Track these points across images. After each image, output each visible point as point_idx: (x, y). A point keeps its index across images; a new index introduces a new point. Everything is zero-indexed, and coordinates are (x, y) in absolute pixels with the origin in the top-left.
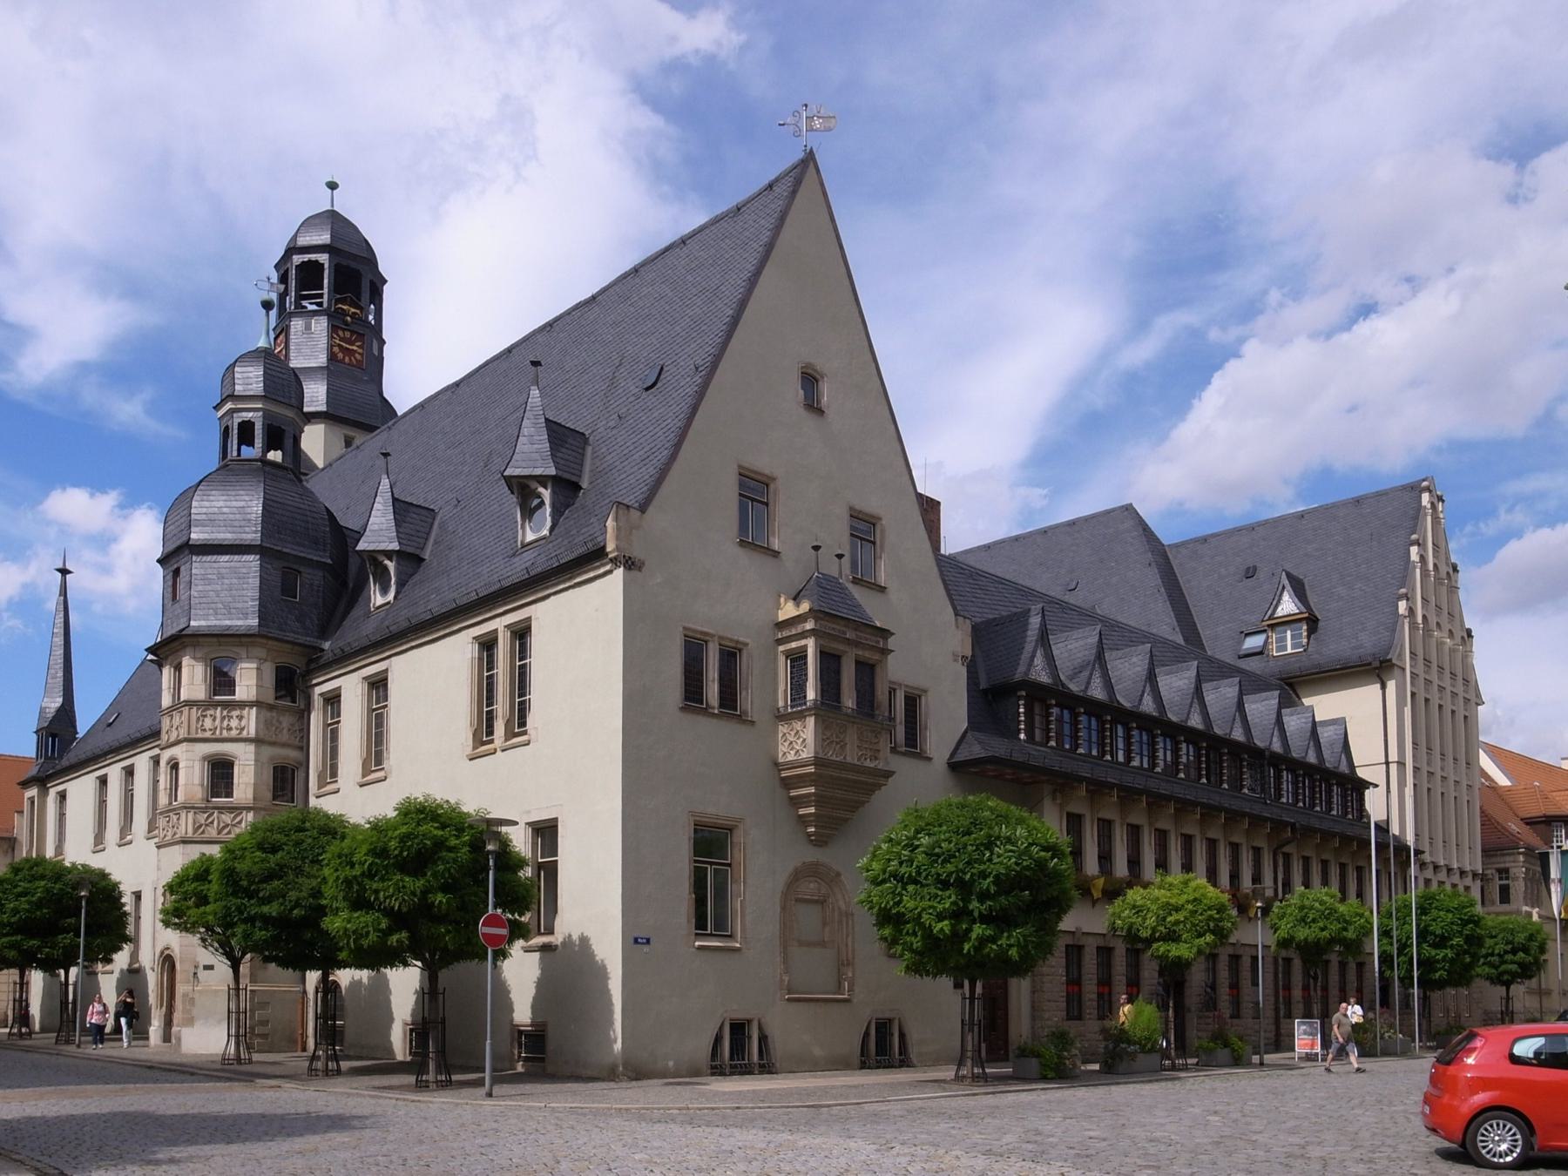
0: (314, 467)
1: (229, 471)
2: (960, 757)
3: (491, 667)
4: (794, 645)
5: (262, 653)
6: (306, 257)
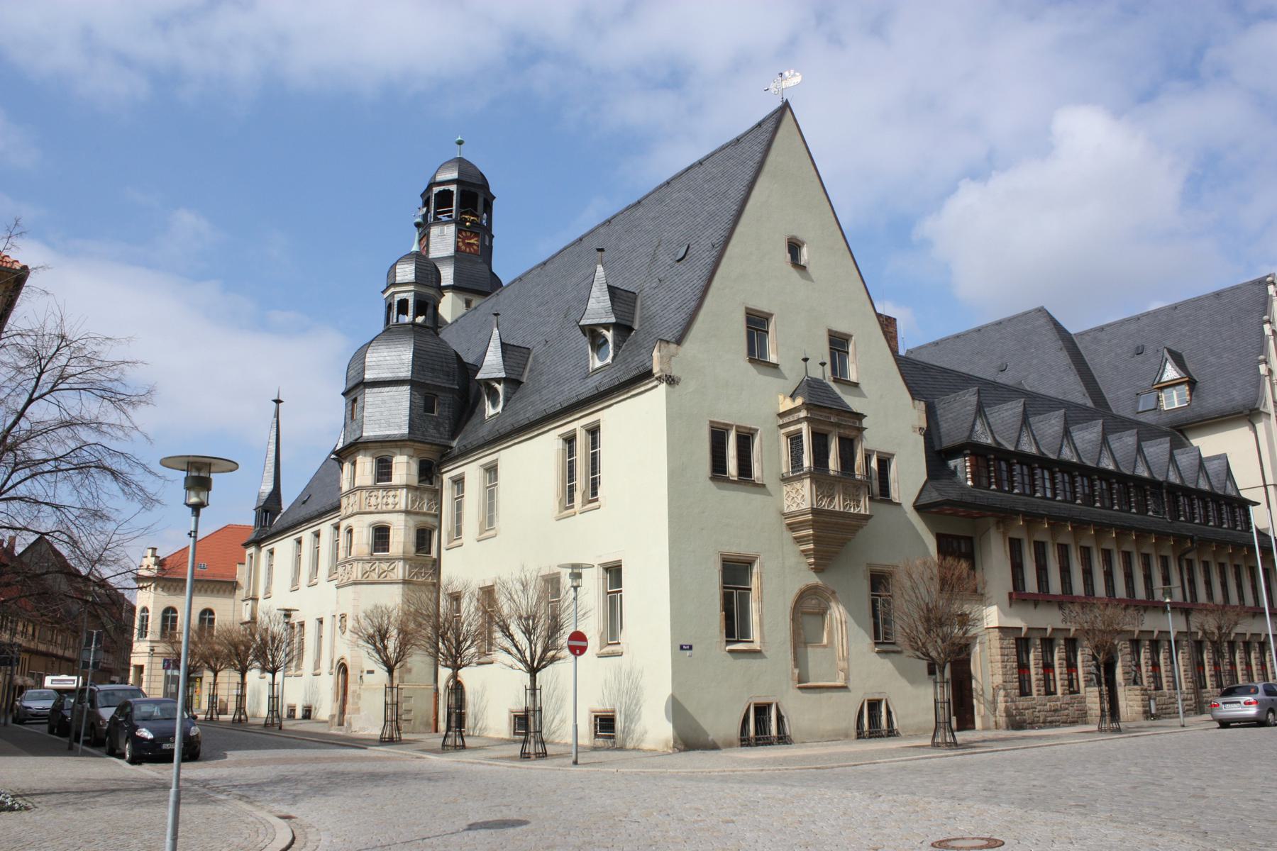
0: (445, 322)
1: (391, 332)
2: (922, 502)
3: (571, 452)
4: (792, 428)
5: (411, 452)
6: (442, 188)
